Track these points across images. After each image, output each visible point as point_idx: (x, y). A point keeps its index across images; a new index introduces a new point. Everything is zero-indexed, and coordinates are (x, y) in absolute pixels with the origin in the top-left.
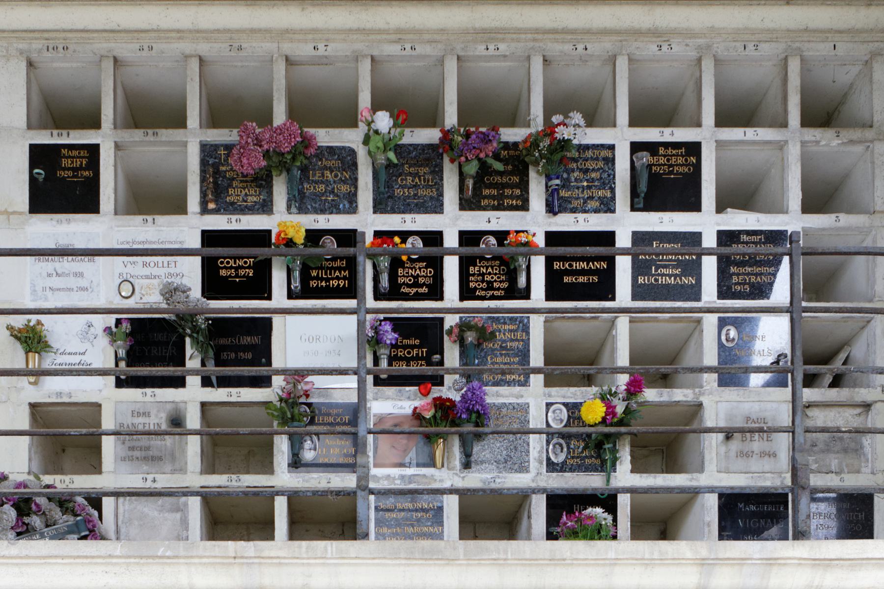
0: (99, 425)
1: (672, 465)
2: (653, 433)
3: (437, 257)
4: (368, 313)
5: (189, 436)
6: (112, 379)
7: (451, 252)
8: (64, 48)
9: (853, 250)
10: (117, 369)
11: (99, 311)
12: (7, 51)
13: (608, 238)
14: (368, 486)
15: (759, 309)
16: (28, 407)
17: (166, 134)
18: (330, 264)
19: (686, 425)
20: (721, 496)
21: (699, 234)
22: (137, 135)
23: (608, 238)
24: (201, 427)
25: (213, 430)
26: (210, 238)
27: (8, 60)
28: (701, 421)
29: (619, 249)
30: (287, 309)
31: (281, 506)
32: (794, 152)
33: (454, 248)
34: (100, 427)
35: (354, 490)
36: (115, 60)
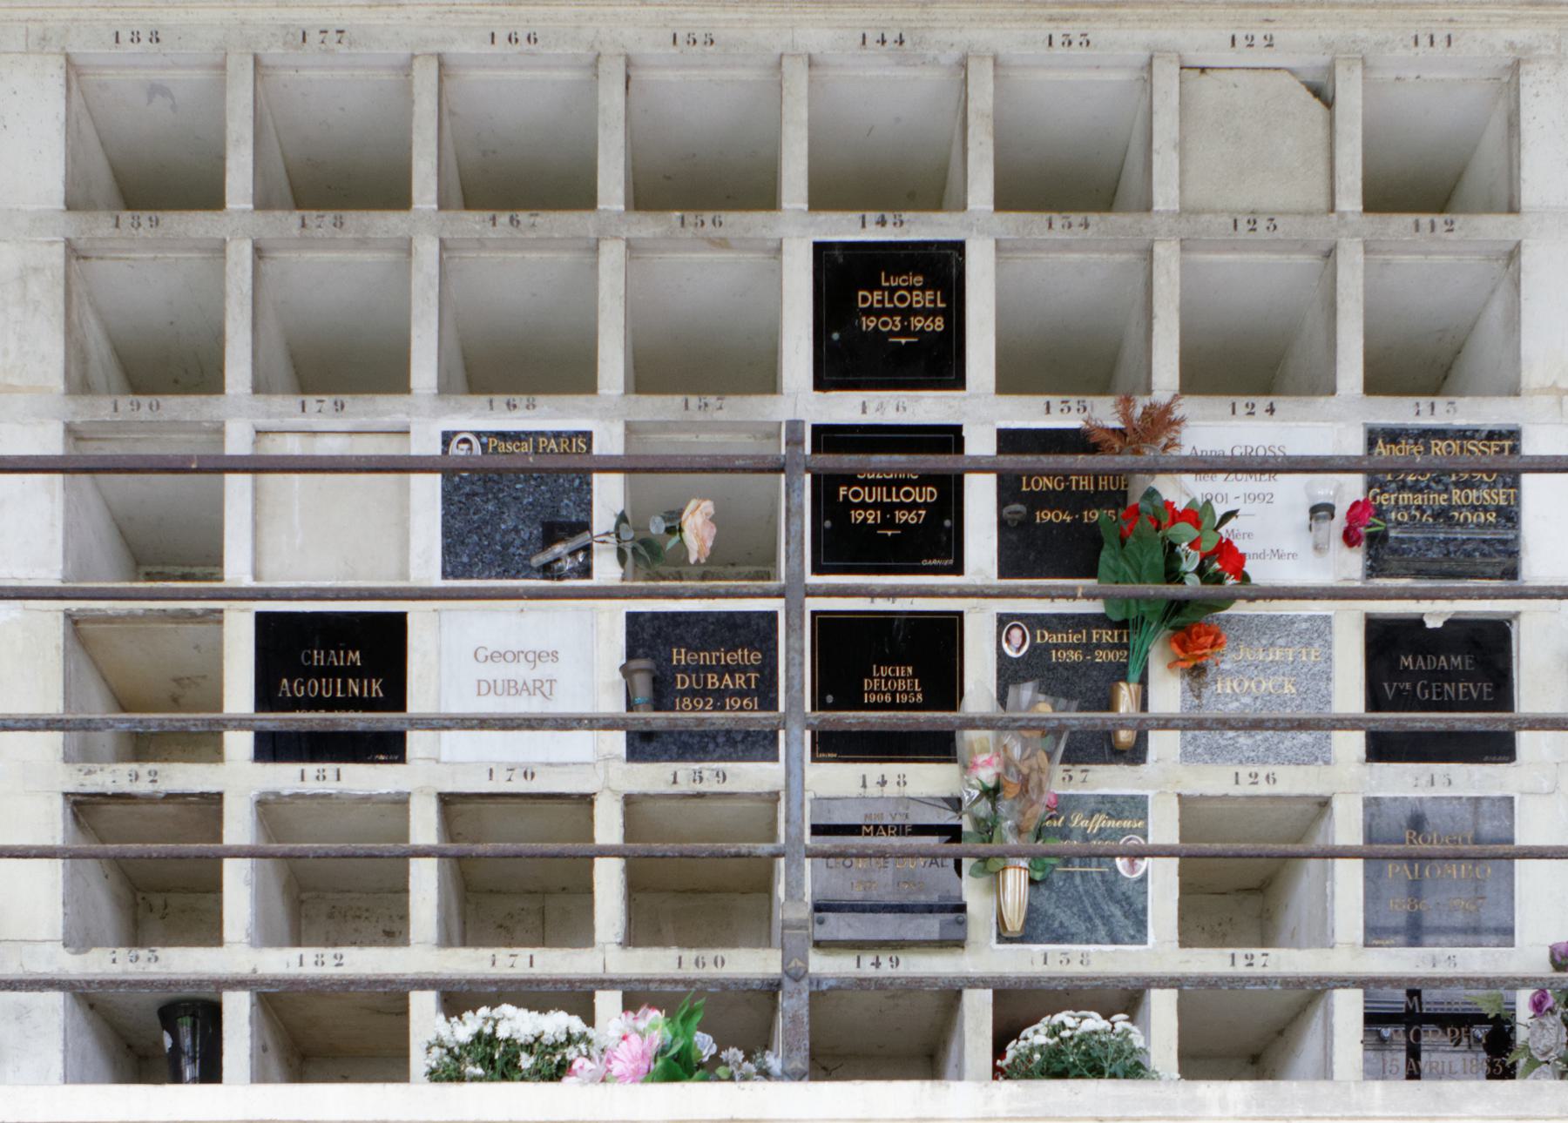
0: (404, 835)
1: (1265, 933)
2: (198, 857)
3: (950, 476)
4: (807, 595)
5: (1338, 862)
6: (617, 741)
7: (980, 467)
8: (529, 38)
9: (325, 466)
10: (1144, 715)
11: (234, 594)
12: (1558, 45)
13: (948, 438)
14: (806, 971)
15: (367, 594)
16: (408, 791)
17: (737, 222)
18: (908, 495)
19: (1298, 841)
20: (998, 995)
21: (956, 430)
22: (290, 221)
23: (948, 438)
24: (440, 840)
25: (465, 847)
26: (1373, 437)
27: (1561, 65)
28: (1326, 836)
29: (974, 458)
30: (1296, 588)
31: (238, 1012)
32: (427, 252)
33: (433, 457)
34: (406, 840)
35: (778, 977)
36: (995, 59)
